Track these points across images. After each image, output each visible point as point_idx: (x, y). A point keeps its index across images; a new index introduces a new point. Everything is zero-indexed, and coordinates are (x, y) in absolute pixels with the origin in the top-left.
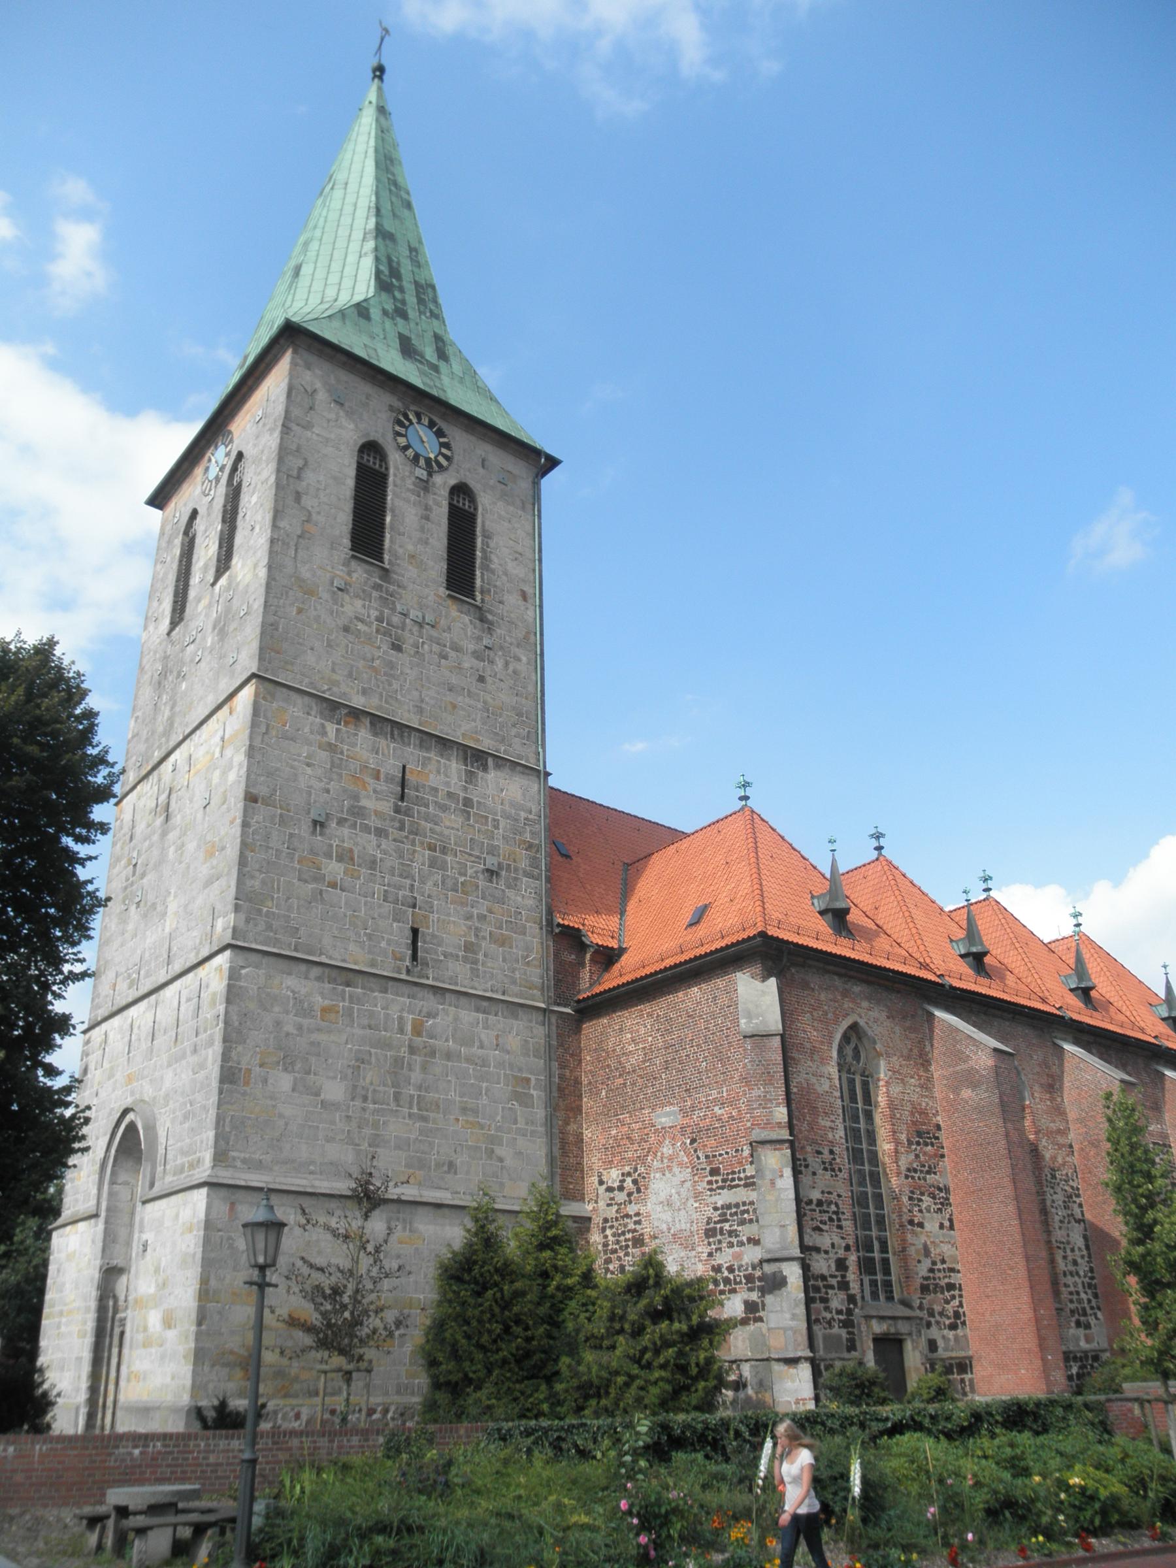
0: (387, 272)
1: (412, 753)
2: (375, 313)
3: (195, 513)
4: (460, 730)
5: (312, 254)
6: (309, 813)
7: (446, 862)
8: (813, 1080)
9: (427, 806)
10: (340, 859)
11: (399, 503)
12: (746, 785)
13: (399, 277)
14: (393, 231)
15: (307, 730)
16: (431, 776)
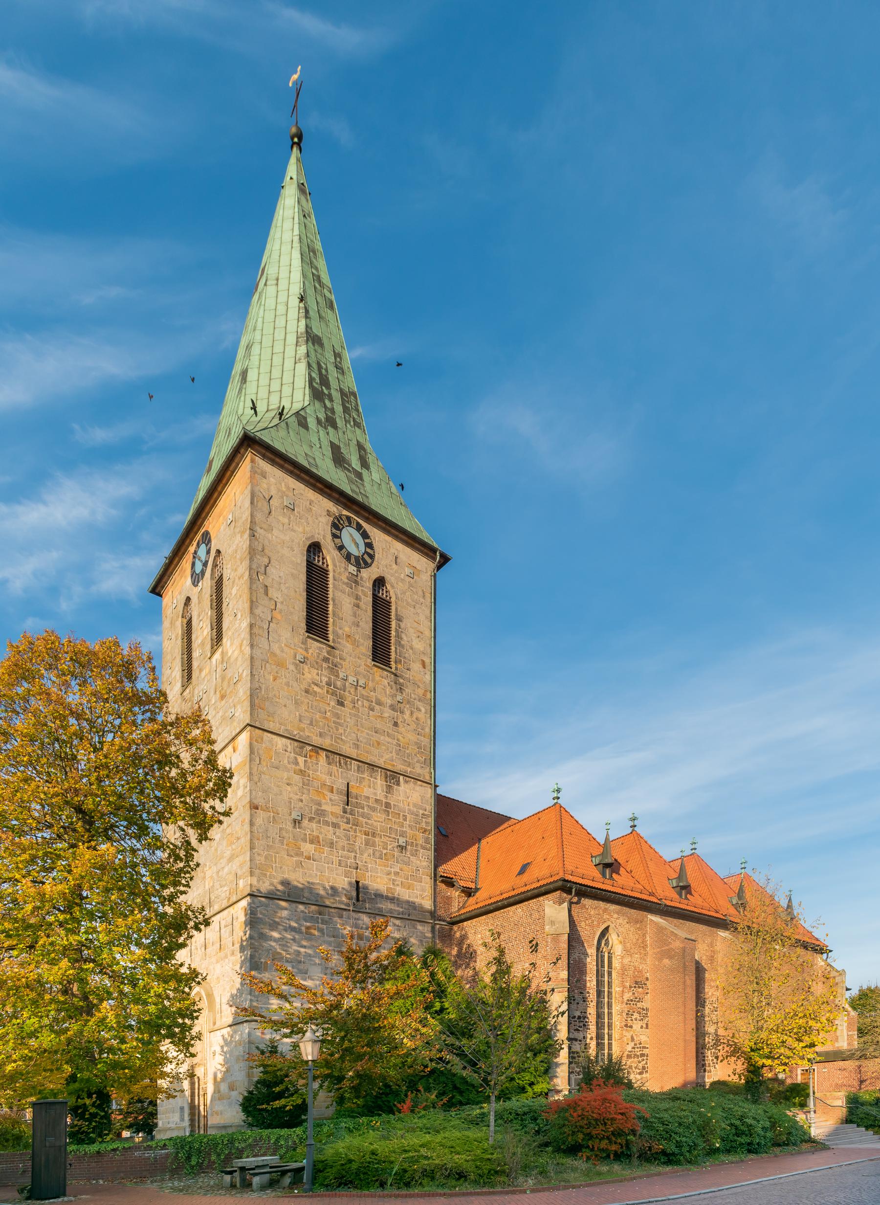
0: (318, 380)
1: (352, 774)
2: (312, 422)
3: (188, 599)
4: (383, 759)
5: (255, 359)
6: (291, 815)
7: (374, 842)
8: (582, 957)
9: (363, 808)
10: (312, 842)
11: (338, 594)
12: (558, 791)
13: (328, 387)
14: (320, 334)
15: (286, 761)
16: (365, 789)
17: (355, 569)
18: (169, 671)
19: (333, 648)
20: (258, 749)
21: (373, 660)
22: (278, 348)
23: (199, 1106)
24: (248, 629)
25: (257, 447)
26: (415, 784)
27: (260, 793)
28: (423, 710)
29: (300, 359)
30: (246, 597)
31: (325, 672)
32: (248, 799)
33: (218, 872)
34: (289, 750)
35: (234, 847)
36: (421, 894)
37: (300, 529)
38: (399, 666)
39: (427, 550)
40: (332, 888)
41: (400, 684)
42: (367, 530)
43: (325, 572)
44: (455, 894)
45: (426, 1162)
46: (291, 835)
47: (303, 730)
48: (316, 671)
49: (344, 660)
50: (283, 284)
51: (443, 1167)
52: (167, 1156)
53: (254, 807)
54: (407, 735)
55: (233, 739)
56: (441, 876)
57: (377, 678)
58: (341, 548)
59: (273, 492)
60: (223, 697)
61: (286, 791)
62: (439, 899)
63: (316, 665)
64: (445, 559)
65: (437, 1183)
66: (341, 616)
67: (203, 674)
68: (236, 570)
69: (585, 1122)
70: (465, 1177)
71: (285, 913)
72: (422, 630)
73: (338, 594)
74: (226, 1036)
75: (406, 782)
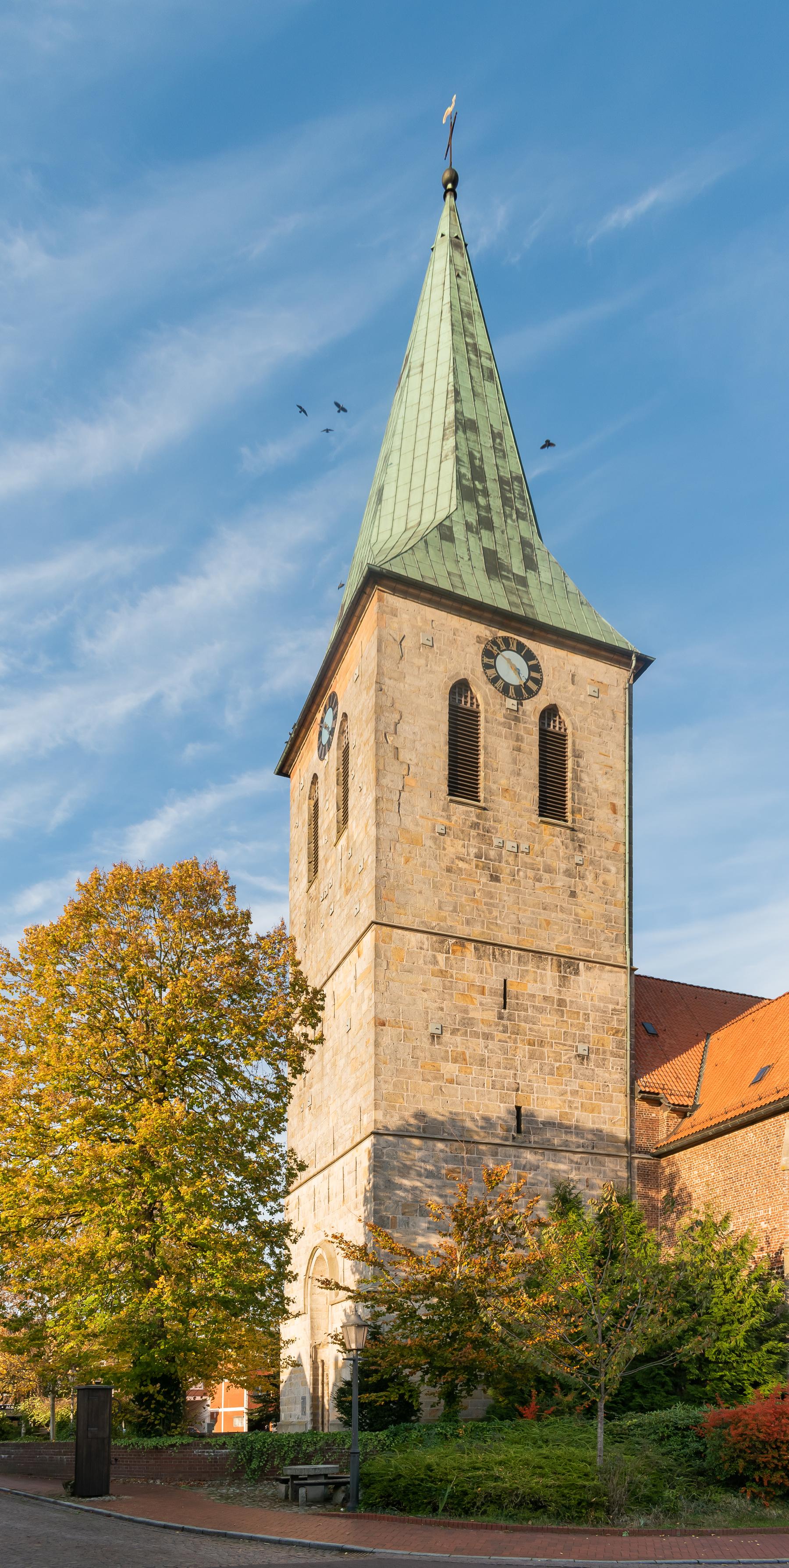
0: (469, 476)
2: (459, 531)
3: (315, 777)
4: (555, 941)
6: (427, 1028)
7: (543, 1053)
9: (526, 1010)
10: (455, 1061)
11: (492, 739)
15: (421, 962)
16: (529, 985)
17: (515, 702)
18: (296, 865)
19: (485, 809)
20: (385, 951)
21: (540, 815)
22: (421, 449)
23: (323, 1397)
24: (374, 805)
25: (385, 582)
26: (602, 970)
27: (388, 1005)
28: (613, 870)
29: (446, 456)
30: (371, 766)
31: (473, 842)
32: (373, 1014)
33: (342, 1106)
34: (425, 947)
35: (358, 1074)
36: (612, 1117)
37: (441, 668)
38: (578, 817)
39: (615, 655)
40: (486, 1119)
41: (580, 840)
42: (532, 648)
43: (475, 715)
44: (662, 1114)
45: (493, 1484)
46: (427, 1054)
47: (444, 919)
48: (461, 842)
49: (500, 822)
50: (429, 369)
51: (512, 1492)
52: (228, 1456)
53: (380, 1023)
54: (590, 906)
55: (358, 941)
56: (641, 1092)
57: (546, 838)
58: (494, 680)
59: (406, 631)
60: (348, 891)
61: (422, 1001)
62: (637, 1123)
63: (463, 835)
64: (644, 663)
65: (505, 1512)
66: (495, 766)
67: (329, 864)
68: (362, 735)
69: (746, 1444)
70: (545, 1507)
71: (418, 1155)
72: (610, 763)
73: (492, 739)
74: (348, 1311)
75: (588, 969)
